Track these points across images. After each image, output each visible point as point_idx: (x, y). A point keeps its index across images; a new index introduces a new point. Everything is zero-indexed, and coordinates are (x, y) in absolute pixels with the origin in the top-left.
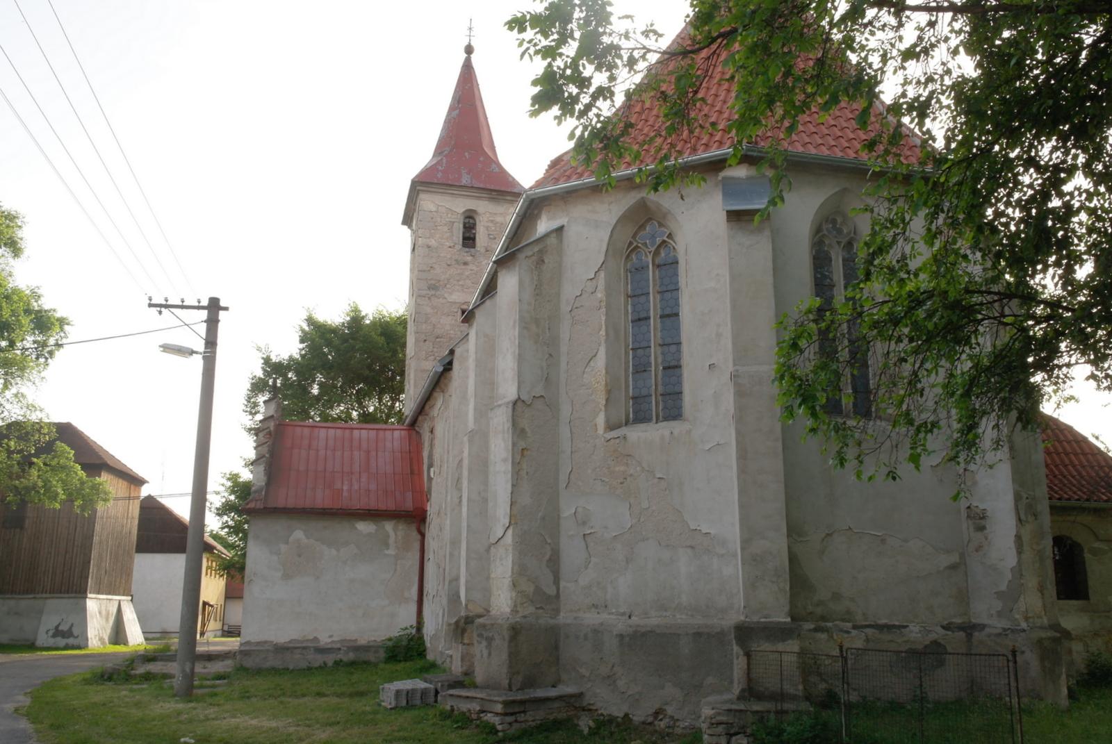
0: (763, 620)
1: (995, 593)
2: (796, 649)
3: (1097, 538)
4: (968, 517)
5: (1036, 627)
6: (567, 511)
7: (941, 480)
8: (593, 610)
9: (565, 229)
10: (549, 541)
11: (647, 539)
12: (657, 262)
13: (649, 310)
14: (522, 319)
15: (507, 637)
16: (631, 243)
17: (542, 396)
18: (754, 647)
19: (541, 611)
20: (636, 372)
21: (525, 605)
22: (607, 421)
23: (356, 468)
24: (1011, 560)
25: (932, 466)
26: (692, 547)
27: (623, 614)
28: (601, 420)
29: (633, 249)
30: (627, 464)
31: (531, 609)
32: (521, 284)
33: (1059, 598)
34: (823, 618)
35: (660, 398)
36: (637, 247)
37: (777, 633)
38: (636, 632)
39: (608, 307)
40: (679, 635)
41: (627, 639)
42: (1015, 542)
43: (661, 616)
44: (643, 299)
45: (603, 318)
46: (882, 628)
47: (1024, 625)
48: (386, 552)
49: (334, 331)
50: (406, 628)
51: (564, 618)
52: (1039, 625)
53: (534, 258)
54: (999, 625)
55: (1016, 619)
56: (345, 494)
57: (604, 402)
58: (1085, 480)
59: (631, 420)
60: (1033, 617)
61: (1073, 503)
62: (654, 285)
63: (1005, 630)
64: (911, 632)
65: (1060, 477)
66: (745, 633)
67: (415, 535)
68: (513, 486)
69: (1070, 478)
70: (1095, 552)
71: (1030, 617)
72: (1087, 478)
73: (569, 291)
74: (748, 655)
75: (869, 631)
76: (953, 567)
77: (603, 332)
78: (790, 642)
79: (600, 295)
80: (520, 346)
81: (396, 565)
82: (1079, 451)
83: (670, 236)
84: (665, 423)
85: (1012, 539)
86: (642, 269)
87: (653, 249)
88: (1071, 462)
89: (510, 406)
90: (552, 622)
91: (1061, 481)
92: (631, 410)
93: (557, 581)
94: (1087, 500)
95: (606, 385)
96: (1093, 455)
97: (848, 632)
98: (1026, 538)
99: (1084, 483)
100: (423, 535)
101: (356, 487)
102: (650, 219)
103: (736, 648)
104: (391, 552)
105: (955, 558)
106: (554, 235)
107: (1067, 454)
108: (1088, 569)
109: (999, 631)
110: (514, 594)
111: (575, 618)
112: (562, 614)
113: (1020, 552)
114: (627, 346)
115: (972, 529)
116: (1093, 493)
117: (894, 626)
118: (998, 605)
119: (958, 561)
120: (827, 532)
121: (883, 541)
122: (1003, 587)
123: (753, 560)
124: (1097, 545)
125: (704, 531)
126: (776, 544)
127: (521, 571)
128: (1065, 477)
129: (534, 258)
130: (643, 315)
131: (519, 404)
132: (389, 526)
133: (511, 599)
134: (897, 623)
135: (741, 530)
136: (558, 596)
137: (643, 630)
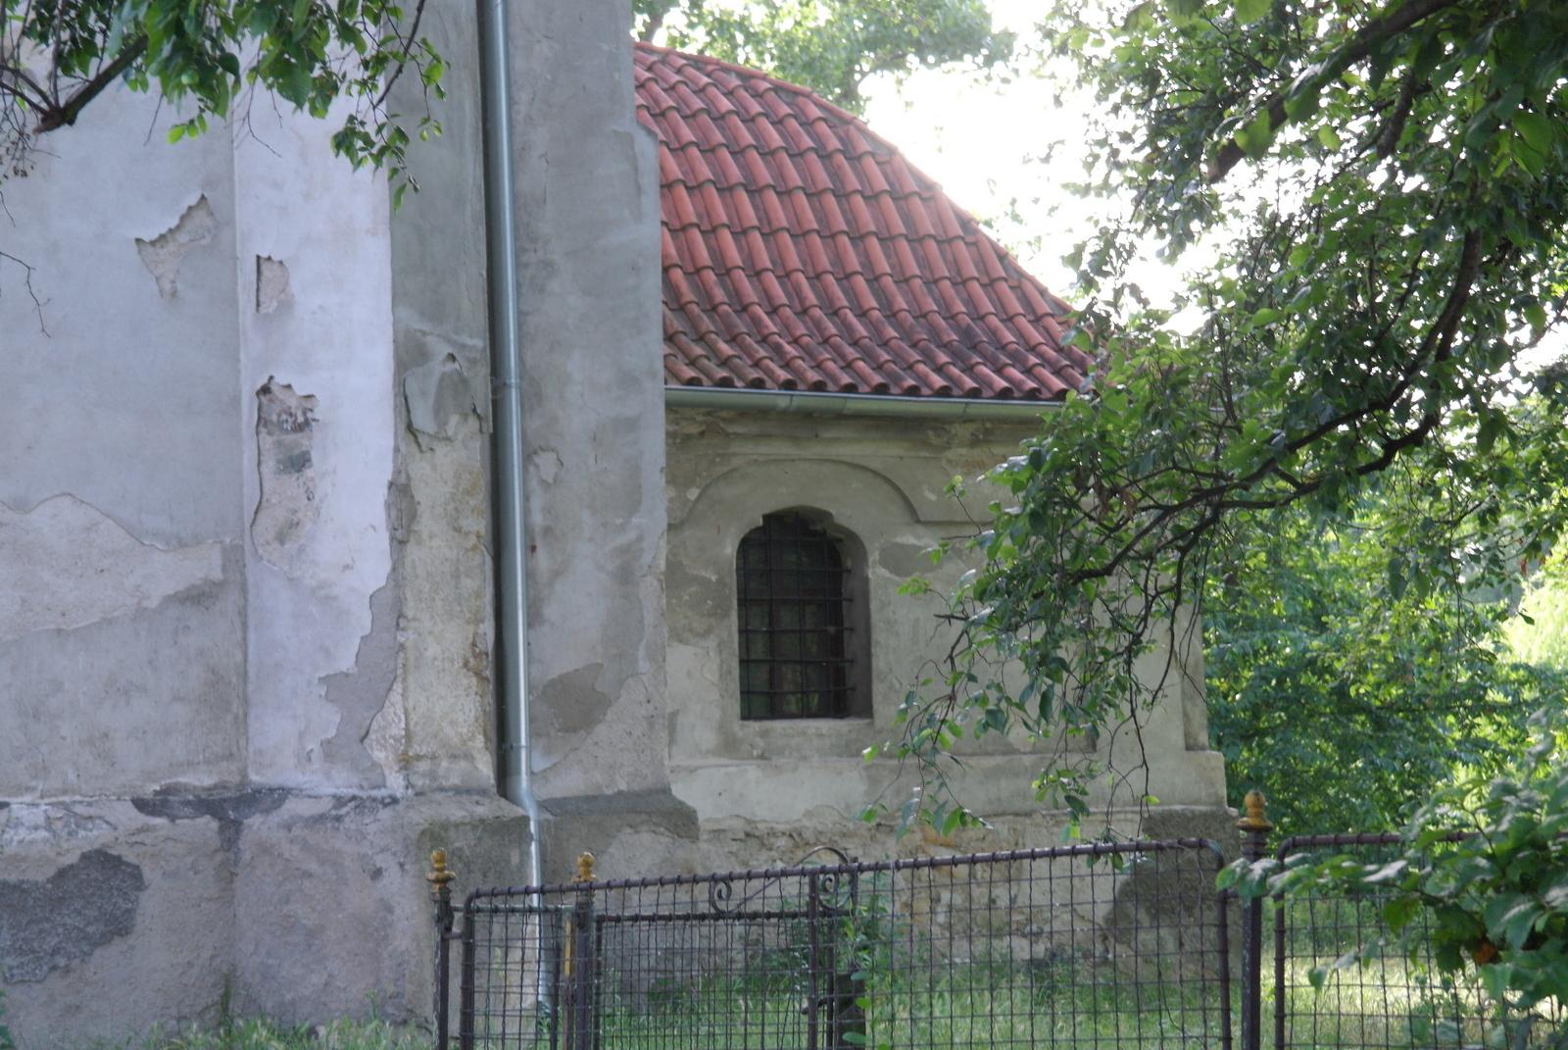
1: (321, 680)
3: (914, 516)
4: (262, 421)
7: (174, 293)
24: (374, 570)
25: (138, 241)
33: (747, 715)
42: (388, 506)
47: (395, 783)
52: (455, 780)
55: (375, 765)
58: (898, 325)
60: (434, 757)
63: (339, 801)
65: (817, 312)
70: (901, 561)
71: (418, 758)
76: (199, 597)
82: (900, 228)
85: (381, 494)
88: (868, 262)
105: (205, 565)
107: (858, 238)
109: (324, 806)
115: (269, 465)
118: (328, 720)
119: (217, 575)
122: (346, 662)
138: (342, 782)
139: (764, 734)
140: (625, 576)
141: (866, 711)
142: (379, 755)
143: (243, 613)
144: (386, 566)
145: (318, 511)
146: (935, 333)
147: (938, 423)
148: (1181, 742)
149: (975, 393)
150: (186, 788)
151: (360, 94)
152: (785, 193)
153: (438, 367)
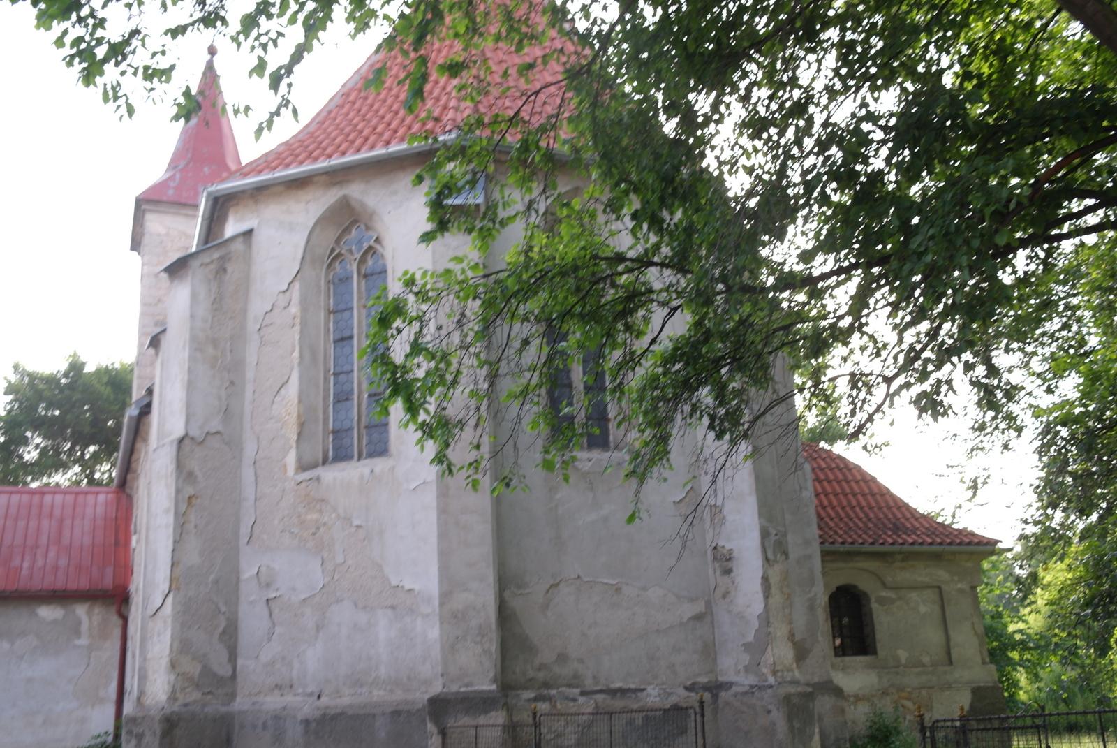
0: (463, 689)
1: (743, 645)
2: (501, 721)
3: (885, 586)
4: (715, 559)
5: (785, 682)
6: (248, 572)
8: (276, 692)
9: (255, 233)
10: (223, 609)
11: (342, 601)
12: (363, 271)
13: (352, 329)
14: (193, 338)
15: (158, 732)
16: (333, 250)
17: (217, 433)
18: (451, 722)
19: (209, 697)
20: (337, 401)
21: (187, 690)
22: (299, 460)
23: (44, 539)
24: (758, 606)
26: (393, 607)
27: (311, 694)
28: (291, 459)
29: (335, 257)
30: (321, 511)
31: (196, 695)
32: (194, 296)
34: (546, 685)
35: (364, 432)
36: (339, 255)
37: (476, 703)
38: (324, 715)
39: (304, 324)
40: (374, 716)
41: (314, 725)
42: (762, 584)
43: (355, 694)
44: (346, 314)
45: (297, 337)
46: (613, 693)
47: (771, 680)
48: (78, 642)
49: (51, 380)
50: (99, 736)
51: (241, 703)
52: (789, 679)
53: (212, 267)
54: (746, 682)
55: (763, 674)
56: (25, 572)
57: (295, 437)
58: (872, 523)
59: (330, 459)
60: (782, 671)
61: (856, 547)
62: (359, 298)
63: (752, 687)
64: (649, 695)
65: (846, 519)
66: (439, 707)
67: (116, 620)
68: (175, 542)
69: (857, 520)
70: (882, 601)
72: (874, 520)
73: (257, 307)
74: (443, 733)
75: (600, 697)
76: (698, 618)
77: (296, 354)
78: (493, 713)
79: (294, 309)
80: (190, 371)
81: (90, 658)
82: (867, 491)
83: (377, 240)
84: (368, 461)
85: (759, 581)
86: (346, 279)
87: (358, 256)
89: (175, 444)
90: (223, 709)
91: (846, 524)
92: (331, 446)
93: (233, 657)
94: (872, 544)
95: (299, 416)
96: (883, 495)
97: (574, 700)
98: (774, 580)
99: (871, 525)
100: (125, 620)
101: (40, 563)
102: (355, 222)
103: (430, 727)
104: (83, 641)
105: (699, 607)
106: (241, 239)
107: (855, 495)
108: (876, 621)
109: (747, 688)
110: (173, 677)
111: (254, 704)
112: (238, 699)
113: (767, 596)
114: (327, 371)
115: (718, 573)
116: (880, 536)
117: (629, 690)
118: (745, 659)
119: (703, 610)
120: (552, 582)
121: (618, 590)
123: (453, 617)
124: (884, 594)
125: (407, 587)
126: (483, 597)
127: (183, 647)
128: (851, 519)
129: (212, 267)
130: (346, 334)
131: (187, 441)
132: (81, 610)
133: (169, 683)
134: (633, 686)
135: (441, 582)
136: (234, 676)
137: (333, 712)
138: (752, 680)
139: (842, 661)
140: (811, 608)
141: (874, 652)
142: (765, 670)
143: (712, 623)
144: (763, 605)
145: (736, 587)
146: (885, 525)
147: (891, 554)
148: (980, 661)
149: (902, 544)
150: (699, 683)
151: (746, 458)
152: (829, 482)
153: (773, 538)
